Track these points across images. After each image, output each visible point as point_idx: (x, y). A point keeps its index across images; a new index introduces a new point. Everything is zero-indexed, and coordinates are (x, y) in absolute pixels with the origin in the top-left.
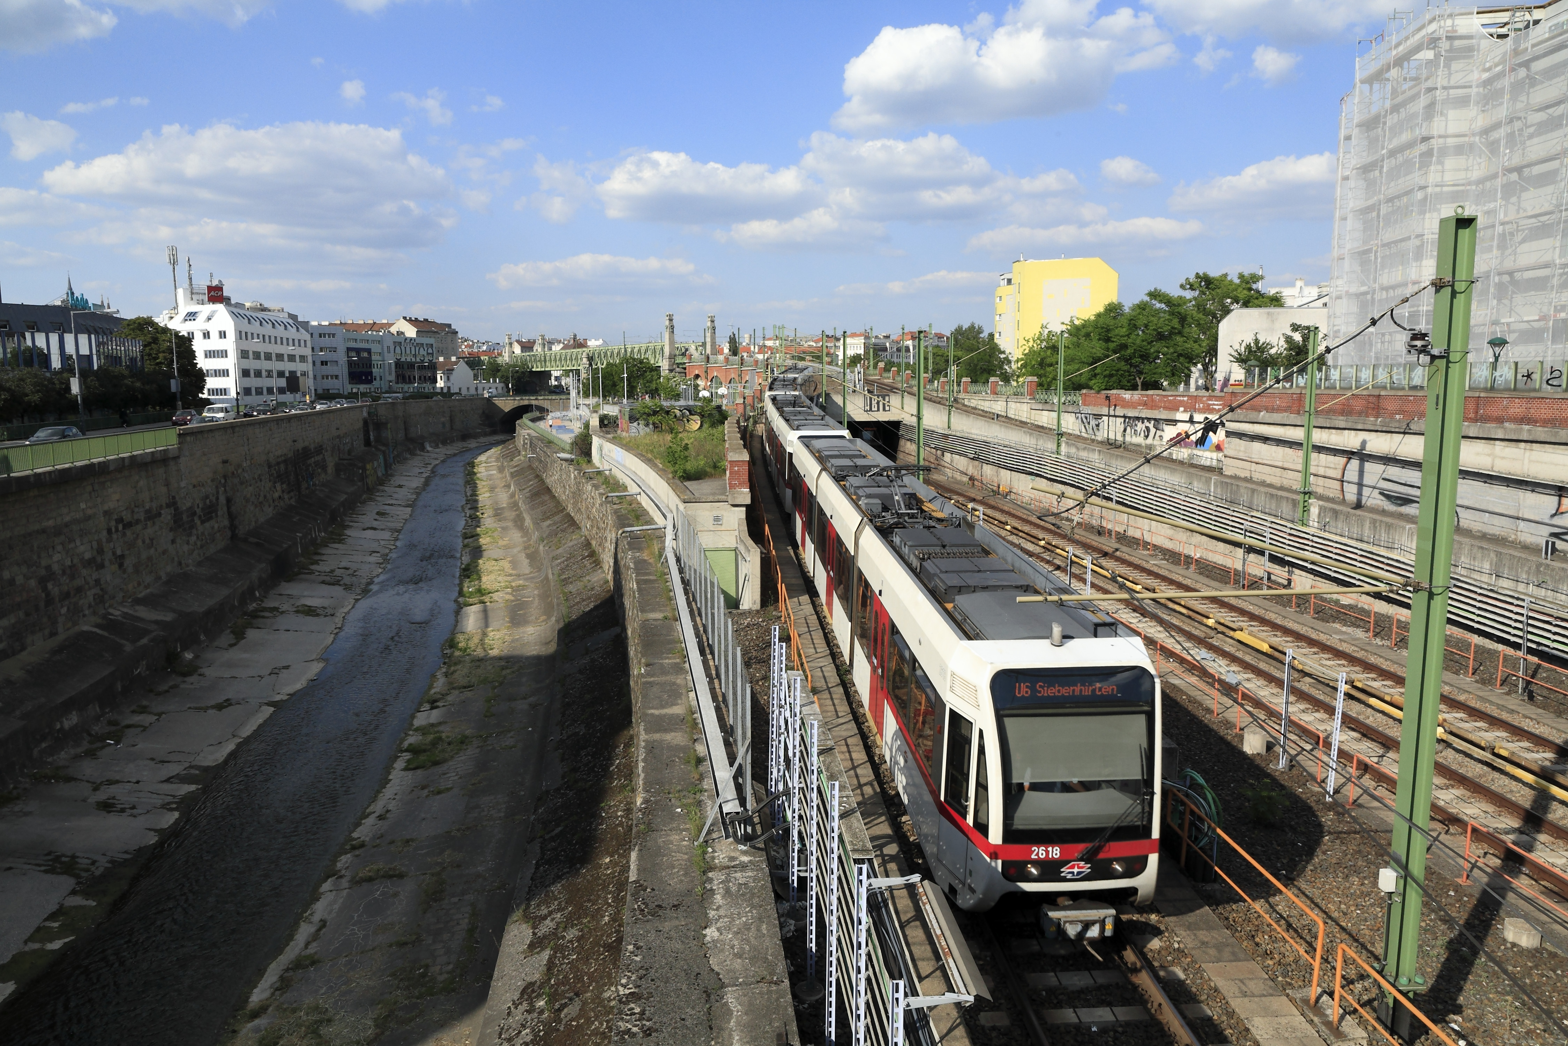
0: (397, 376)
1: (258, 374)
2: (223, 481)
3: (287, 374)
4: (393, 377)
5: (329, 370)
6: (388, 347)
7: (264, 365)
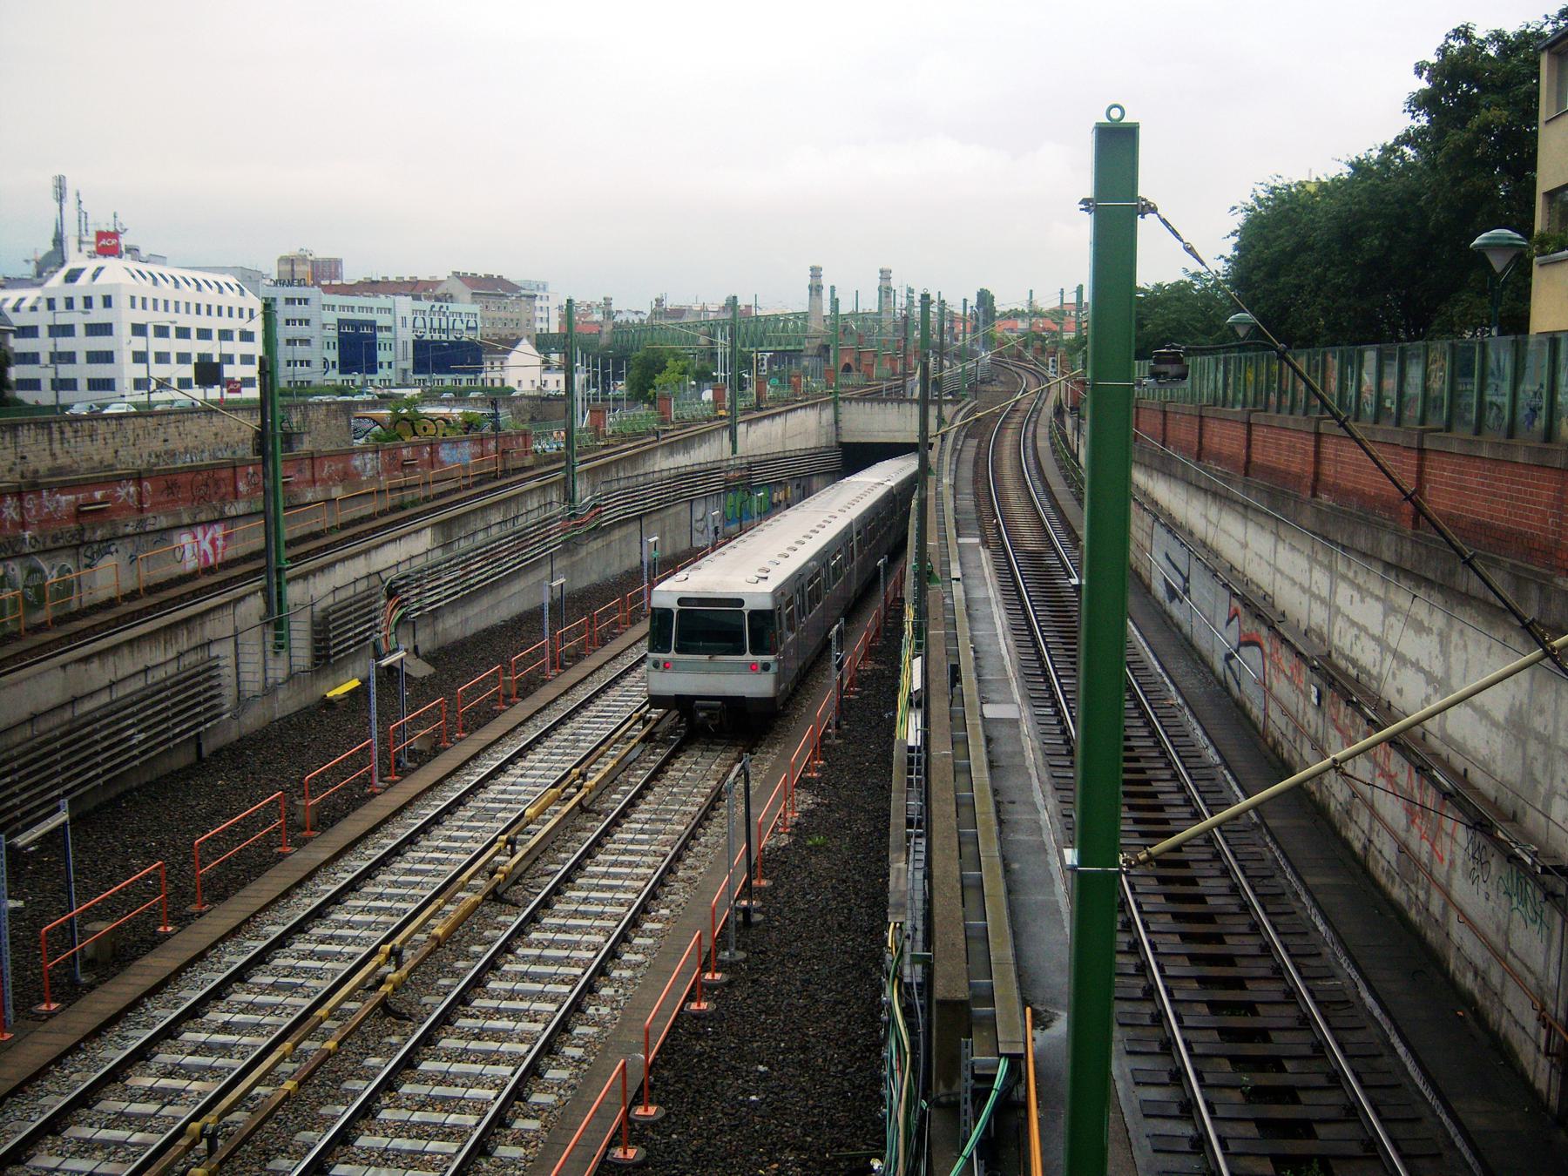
3: (195, 359)
4: (409, 364)
6: (404, 319)
7: (156, 345)
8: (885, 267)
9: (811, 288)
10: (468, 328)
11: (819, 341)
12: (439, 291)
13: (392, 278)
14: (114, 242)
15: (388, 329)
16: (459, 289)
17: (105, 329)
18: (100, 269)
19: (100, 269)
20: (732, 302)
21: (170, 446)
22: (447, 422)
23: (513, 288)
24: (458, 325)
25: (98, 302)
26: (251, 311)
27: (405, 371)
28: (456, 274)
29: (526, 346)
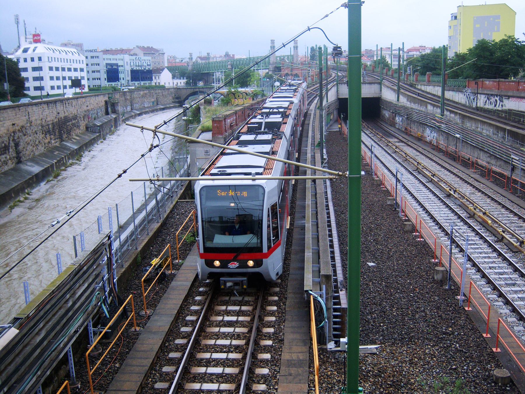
0: (132, 78)
1: (58, 78)
2: (13, 134)
4: (129, 78)
5: (96, 75)
6: (127, 62)
7: (59, 74)
8: (273, 39)
9: (271, 47)
11: (274, 65)
12: (132, 53)
13: (114, 49)
14: (39, 38)
15: (122, 66)
16: (138, 51)
17: (40, 69)
18: (36, 47)
19: (36, 47)
20: (227, 55)
21: (88, 108)
22: (246, 94)
23: (157, 51)
24: (145, 64)
25: (36, 59)
26: (83, 61)
27: (128, 81)
28: (137, 46)
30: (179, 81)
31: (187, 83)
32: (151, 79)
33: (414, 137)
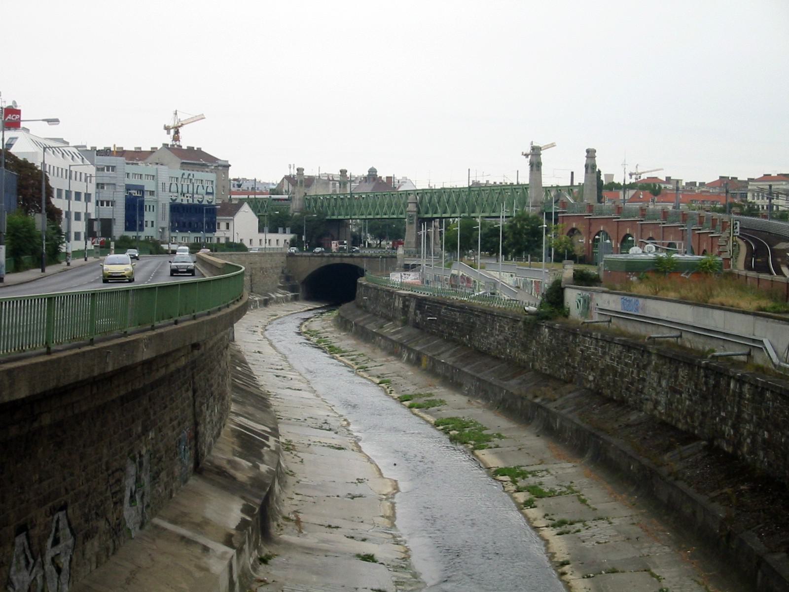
0: (172, 221)
4: (166, 223)
6: (164, 184)
8: (591, 147)
9: (587, 166)
10: (207, 193)
20: (372, 175)
27: (163, 229)
29: (246, 207)
30: (273, 237)
31: (293, 243)
32: (212, 227)
33: (356, 497)
